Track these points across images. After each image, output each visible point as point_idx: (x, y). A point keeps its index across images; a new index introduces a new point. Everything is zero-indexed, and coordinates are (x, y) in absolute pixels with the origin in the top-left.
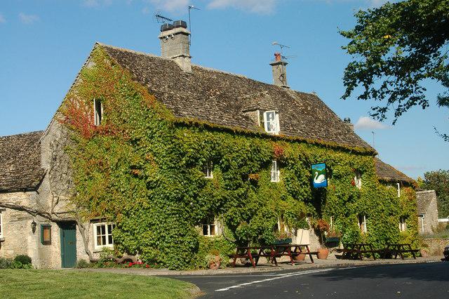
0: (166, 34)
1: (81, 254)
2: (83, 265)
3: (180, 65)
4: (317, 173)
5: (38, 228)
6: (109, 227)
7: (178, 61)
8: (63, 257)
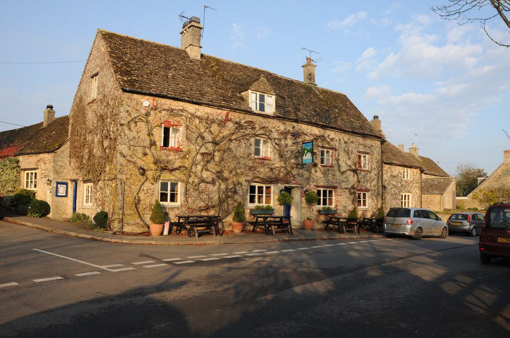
4: (306, 151)
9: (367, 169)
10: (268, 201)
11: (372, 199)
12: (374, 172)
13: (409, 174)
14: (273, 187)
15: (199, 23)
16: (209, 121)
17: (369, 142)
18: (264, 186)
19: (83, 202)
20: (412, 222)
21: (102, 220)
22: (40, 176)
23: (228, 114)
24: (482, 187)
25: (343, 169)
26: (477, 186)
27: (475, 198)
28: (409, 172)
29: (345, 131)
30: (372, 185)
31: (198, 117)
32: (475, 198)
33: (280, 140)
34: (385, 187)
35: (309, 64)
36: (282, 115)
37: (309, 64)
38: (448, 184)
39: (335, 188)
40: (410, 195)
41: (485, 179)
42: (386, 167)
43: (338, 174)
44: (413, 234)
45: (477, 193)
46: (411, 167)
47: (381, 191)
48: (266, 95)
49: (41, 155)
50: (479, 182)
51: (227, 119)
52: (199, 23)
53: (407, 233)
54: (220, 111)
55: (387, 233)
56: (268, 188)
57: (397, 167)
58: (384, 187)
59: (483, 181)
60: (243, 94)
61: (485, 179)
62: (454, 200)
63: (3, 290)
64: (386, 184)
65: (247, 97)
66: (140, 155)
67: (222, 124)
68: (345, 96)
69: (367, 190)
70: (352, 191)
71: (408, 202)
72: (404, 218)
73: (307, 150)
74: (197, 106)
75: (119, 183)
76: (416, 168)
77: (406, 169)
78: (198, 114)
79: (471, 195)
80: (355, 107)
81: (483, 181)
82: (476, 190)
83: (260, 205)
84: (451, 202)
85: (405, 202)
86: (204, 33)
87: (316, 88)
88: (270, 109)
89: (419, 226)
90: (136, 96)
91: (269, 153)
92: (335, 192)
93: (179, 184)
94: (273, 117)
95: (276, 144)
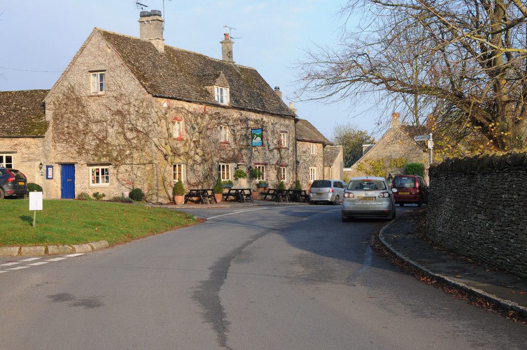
0: (144, 19)
1: (78, 191)
2: (83, 197)
3: (155, 45)
4: (255, 136)
5: (44, 168)
6: (103, 170)
7: (153, 42)
8: (62, 190)
9: (285, 146)
10: (228, 178)
11: (290, 173)
12: (291, 149)
13: (314, 149)
14: (230, 165)
15: (160, 16)
16: (195, 115)
17: (287, 122)
18: (225, 165)
19: (89, 183)
20: (333, 191)
21: (136, 195)
22: (32, 158)
23: (205, 107)
24: (367, 156)
25: (271, 147)
26: (361, 155)
27: (360, 169)
28: (314, 147)
29: (272, 115)
30: (289, 160)
31: (191, 113)
32: (360, 169)
33: (233, 126)
34: (298, 162)
35: (227, 41)
36: (236, 104)
37: (227, 41)
38: (336, 155)
39: (266, 164)
40: (315, 168)
41: (371, 147)
42: (299, 143)
43: (267, 152)
44: (333, 200)
45: (362, 163)
46: (316, 142)
47: (295, 166)
48: (224, 88)
49: (20, 139)
50: (364, 150)
51: (205, 112)
52: (160, 16)
53: (329, 200)
54: (201, 106)
55: (312, 201)
56: (227, 166)
57: (306, 143)
58: (297, 162)
59: (369, 149)
60: (208, 88)
61: (371, 147)
62: (342, 172)
63: (3, 268)
64: (298, 159)
65: (213, 90)
66: (164, 145)
67: (202, 116)
68: (256, 71)
69: (286, 166)
70: (277, 166)
71: (228, 173)
72: (327, 188)
73: (257, 135)
74: (189, 103)
75: (155, 166)
76: (320, 142)
77: (312, 144)
78: (191, 110)
79: (355, 165)
80: (267, 84)
81: (369, 149)
82: (362, 160)
83: (262, 180)
84: (339, 175)
85: (223, 173)
86: (166, 25)
87: (235, 66)
88: (226, 101)
89: (337, 194)
90: (159, 99)
91: (227, 138)
92: (266, 168)
93: (182, 165)
94: (228, 108)
95: (232, 130)
